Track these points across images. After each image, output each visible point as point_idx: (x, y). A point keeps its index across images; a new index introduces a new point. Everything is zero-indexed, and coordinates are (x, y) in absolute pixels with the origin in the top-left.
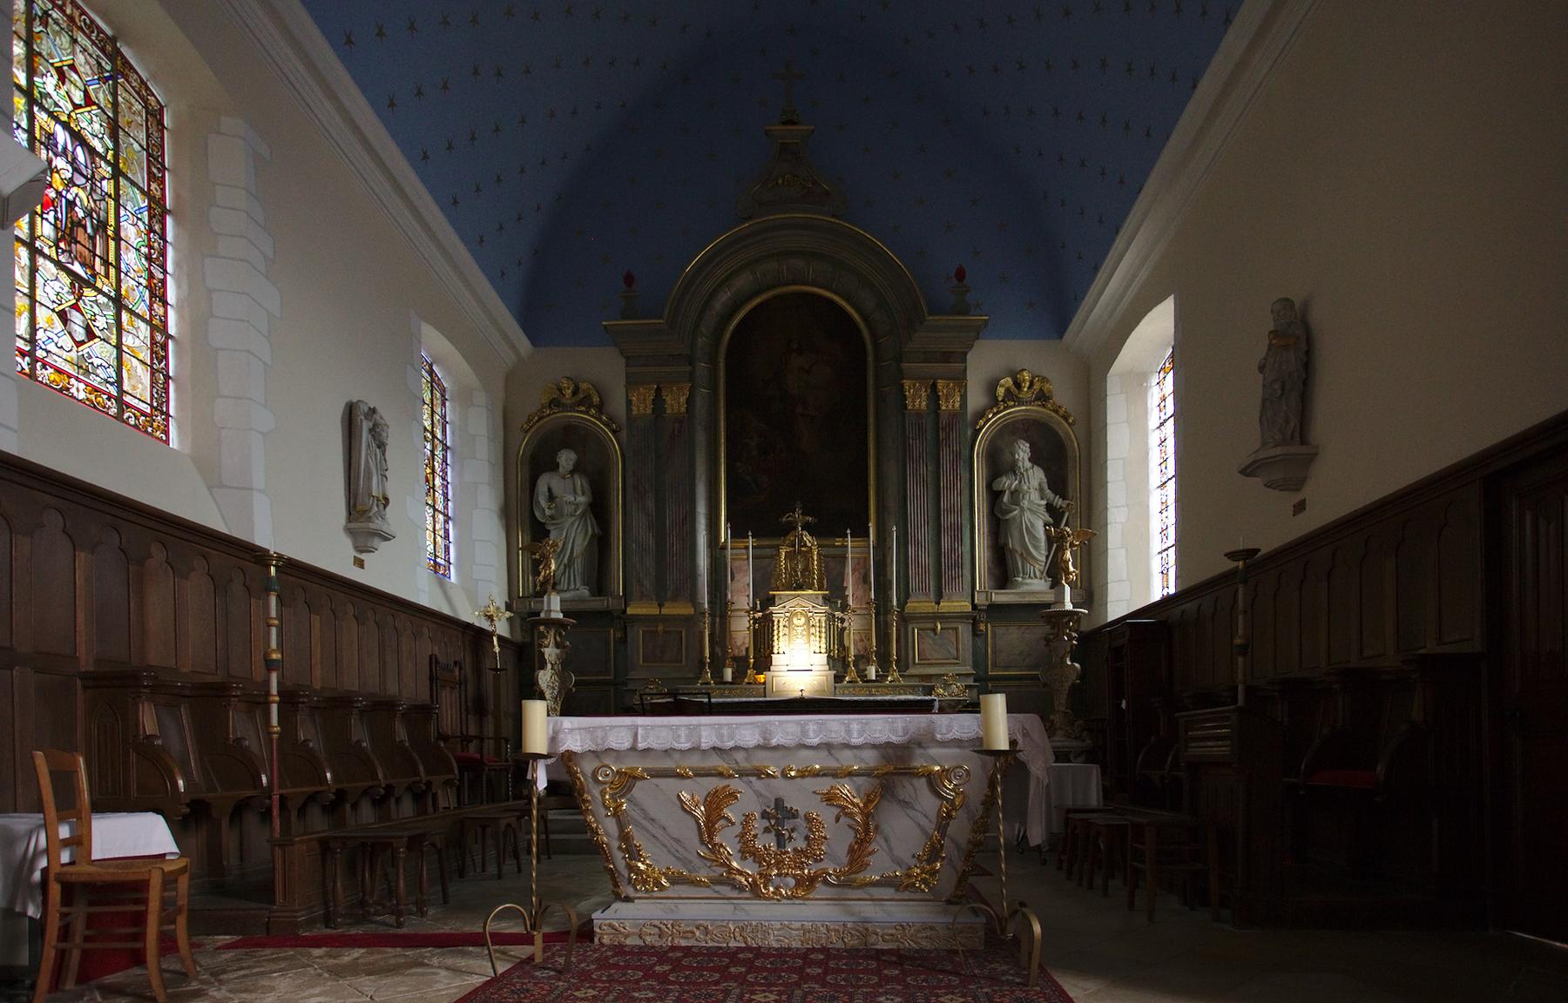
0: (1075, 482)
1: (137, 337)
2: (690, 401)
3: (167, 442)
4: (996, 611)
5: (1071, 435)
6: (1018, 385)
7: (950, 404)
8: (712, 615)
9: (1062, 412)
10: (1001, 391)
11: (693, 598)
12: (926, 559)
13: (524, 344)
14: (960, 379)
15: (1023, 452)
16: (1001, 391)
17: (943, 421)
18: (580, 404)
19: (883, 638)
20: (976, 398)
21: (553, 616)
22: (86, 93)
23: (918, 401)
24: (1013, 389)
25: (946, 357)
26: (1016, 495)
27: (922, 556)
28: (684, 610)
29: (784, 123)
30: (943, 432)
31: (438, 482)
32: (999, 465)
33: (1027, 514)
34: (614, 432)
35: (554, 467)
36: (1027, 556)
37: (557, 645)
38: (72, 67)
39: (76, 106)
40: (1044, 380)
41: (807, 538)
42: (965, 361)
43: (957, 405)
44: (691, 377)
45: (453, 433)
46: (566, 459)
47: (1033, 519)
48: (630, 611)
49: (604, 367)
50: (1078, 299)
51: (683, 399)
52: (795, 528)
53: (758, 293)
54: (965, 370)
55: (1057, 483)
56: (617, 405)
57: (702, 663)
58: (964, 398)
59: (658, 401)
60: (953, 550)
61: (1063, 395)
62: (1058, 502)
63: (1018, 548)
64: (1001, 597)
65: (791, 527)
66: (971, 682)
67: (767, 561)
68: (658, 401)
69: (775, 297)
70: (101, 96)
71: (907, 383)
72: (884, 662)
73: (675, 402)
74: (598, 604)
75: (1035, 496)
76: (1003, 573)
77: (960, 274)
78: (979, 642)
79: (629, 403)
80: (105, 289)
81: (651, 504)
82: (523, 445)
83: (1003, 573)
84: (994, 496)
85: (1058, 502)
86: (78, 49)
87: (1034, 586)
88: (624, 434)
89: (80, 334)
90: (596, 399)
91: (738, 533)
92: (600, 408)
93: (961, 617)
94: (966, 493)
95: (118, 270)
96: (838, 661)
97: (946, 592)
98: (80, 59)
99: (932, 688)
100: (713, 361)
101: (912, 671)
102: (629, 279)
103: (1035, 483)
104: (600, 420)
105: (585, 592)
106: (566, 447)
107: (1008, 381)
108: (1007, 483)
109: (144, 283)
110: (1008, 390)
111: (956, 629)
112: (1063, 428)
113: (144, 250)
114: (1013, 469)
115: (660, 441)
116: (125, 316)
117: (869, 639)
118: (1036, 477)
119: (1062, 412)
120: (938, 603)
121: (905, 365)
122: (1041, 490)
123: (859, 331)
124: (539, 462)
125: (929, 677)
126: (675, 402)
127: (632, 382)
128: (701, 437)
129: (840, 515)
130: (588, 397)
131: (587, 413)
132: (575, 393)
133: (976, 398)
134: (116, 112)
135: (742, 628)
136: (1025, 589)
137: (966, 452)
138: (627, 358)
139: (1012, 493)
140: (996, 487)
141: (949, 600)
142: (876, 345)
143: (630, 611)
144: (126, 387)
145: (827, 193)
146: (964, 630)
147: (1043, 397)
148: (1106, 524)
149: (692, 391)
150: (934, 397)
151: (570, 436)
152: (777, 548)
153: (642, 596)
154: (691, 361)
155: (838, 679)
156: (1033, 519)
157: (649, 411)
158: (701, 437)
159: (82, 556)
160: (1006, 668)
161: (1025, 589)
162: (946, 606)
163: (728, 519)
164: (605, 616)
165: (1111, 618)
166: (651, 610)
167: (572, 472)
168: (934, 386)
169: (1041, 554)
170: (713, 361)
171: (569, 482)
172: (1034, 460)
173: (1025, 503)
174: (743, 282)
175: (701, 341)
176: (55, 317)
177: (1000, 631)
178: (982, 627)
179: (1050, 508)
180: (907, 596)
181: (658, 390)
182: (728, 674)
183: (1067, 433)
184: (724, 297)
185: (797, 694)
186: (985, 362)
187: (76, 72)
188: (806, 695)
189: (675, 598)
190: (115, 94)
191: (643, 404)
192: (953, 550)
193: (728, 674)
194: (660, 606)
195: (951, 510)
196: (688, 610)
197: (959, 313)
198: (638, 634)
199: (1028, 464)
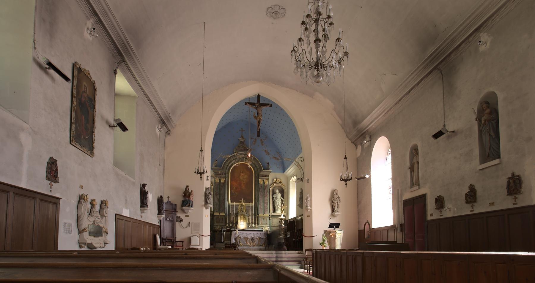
4: (273, 216)
5: (285, 191)
7: (266, 183)
12: (262, 207)
14: (268, 179)
15: (277, 191)
20: (270, 181)
25: (266, 176)
26: (276, 198)
27: (261, 207)
32: (274, 193)
36: (278, 208)
47: (279, 201)
55: (283, 196)
59: (220, 180)
64: (274, 214)
68: (220, 180)
72: (255, 224)
76: (274, 211)
77: (268, 164)
83: (274, 211)
84: (273, 198)
96: (248, 224)
108: (275, 196)
112: (283, 187)
118: (280, 195)
126: (223, 181)
128: (226, 186)
133: (270, 181)
135: (232, 218)
146: (268, 219)
147: (280, 182)
148: (392, 162)
150: (264, 182)
156: (279, 201)
159: (292, 214)
165: (290, 218)
166: (218, 214)
182: (231, 225)
186: (271, 176)
193: (231, 225)
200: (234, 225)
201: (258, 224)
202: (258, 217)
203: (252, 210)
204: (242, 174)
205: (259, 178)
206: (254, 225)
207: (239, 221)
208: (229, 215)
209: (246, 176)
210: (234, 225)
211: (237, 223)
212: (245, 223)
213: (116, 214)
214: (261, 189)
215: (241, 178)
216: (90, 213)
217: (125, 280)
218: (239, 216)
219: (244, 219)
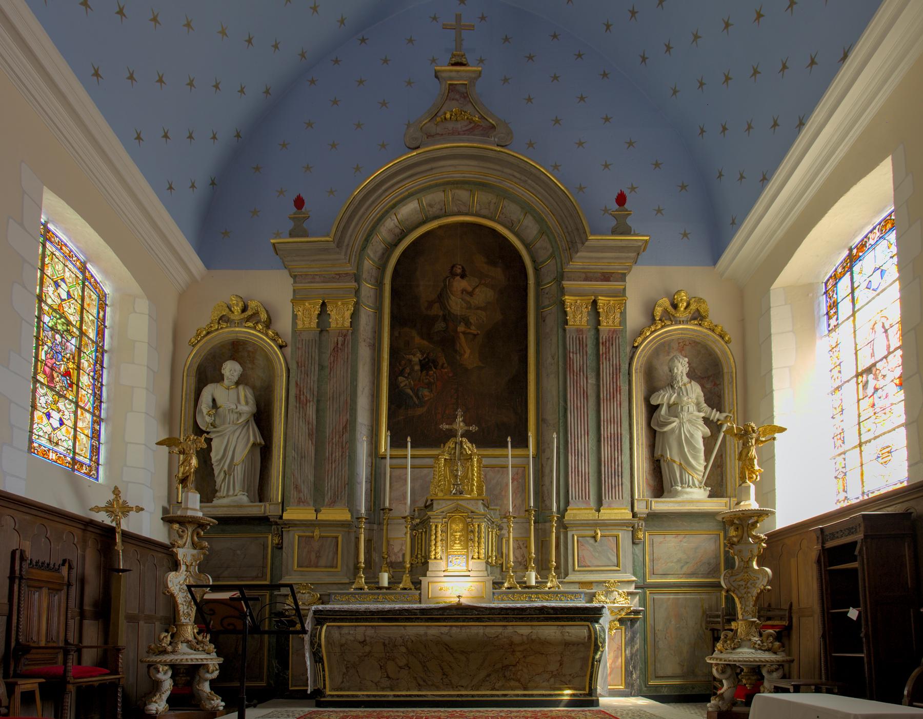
0: (731, 396)
1: (86, 420)
2: (355, 316)
3: (97, 479)
4: (654, 518)
5: (729, 354)
6: (675, 306)
8: (369, 521)
9: (718, 330)
10: (658, 311)
11: (351, 505)
12: (588, 467)
13: (196, 264)
15: (681, 367)
16: (658, 311)
17: (603, 336)
18: (248, 319)
19: (543, 545)
20: (634, 316)
21: (190, 513)
22: (68, 293)
23: (578, 318)
24: (670, 309)
25: (606, 277)
26: (674, 410)
27: (583, 465)
28: (342, 515)
29: (453, 65)
30: (600, 344)
31: (85, 380)
33: (687, 426)
34: (281, 347)
35: (220, 378)
36: (686, 465)
37: (194, 545)
38: (63, 280)
39: (63, 300)
40: (700, 300)
41: (468, 447)
42: (625, 281)
43: (617, 321)
44: (357, 292)
45: (111, 337)
46: (231, 369)
48: (286, 516)
49: (273, 289)
50: (736, 224)
51: (348, 314)
52: (455, 436)
53: (424, 222)
54: (624, 289)
55: (714, 400)
56: (284, 324)
57: (357, 568)
58: (623, 314)
60: (612, 459)
61: (719, 312)
62: (715, 415)
63: (677, 459)
64: (662, 505)
65: (451, 434)
66: (632, 589)
67: (425, 471)
69: (440, 227)
70: (76, 293)
71: (568, 299)
72: (543, 568)
73: (340, 317)
74: (257, 510)
75: (693, 408)
76: (660, 484)
78: (638, 549)
79: (295, 317)
80: (71, 398)
81: (311, 411)
82: (190, 357)
83: (660, 484)
84: (652, 409)
85: (715, 415)
86: (67, 270)
87: (694, 496)
88: (288, 350)
89: (56, 424)
90: (263, 316)
91: (397, 442)
92: (268, 324)
93: (621, 524)
94: (625, 404)
95: (78, 386)
96: (497, 570)
97: (605, 501)
98: (68, 274)
99: (594, 595)
100: (379, 284)
101: (572, 577)
102: (299, 203)
103: (693, 396)
104: (267, 335)
105: (244, 499)
106: (233, 358)
107: (665, 302)
108: (663, 398)
109: (90, 392)
110: (665, 311)
111: (617, 537)
112: (719, 346)
113: (92, 374)
114: (671, 384)
115: (324, 348)
116: (79, 411)
117: (528, 547)
118: (695, 392)
119: (718, 330)
120: (599, 511)
121: (566, 283)
122: (698, 404)
123: (520, 258)
124: (207, 373)
125: (590, 584)
127: (296, 300)
129: (503, 424)
130: (256, 314)
131: (254, 328)
132: (244, 310)
134: (83, 300)
135: (400, 539)
136: (685, 497)
137: (625, 367)
138: (294, 277)
139: (669, 406)
140: (654, 402)
141: (610, 507)
142: (537, 270)
143: (286, 516)
144: (77, 451)
145: (493, 127)
146: (625, 537)
147: (698, 317)
149: (357, 305)
151: (236, 350)
152: (436, 457)
153: (301, 502)
154: (357, 278)
155: (497, 584)
157: (314, 325)
158: (364, 352)
160: (665, 575)
161: (685, 497)
162: (606, 514)
163: (389, 428)
164: (263, 521)
165: (777, 528)
166: (307, 514)
167: (237, 384)
168: (595, 303)
169: (699, 464)
170: (379, 284)
171: (233, 393)
172: (691, 375)
173: (685, 416)
174: (409, 209)
175: (368, 264)
176: (44, 416)
177: (658, 539)
178: (640, 535)
179: (707, 421)
180: (567, 503)
181: (324, 305)
182: (385, 579)
183: (724, 353)
184: (390, 223)
185: (455, 601)
186: (642, 284)
187: (65, 282)
188: (464, 601)
189: (333, 503)
190: (83, 291)
191: (308, 321)
192: (612, 459)
193: (385, 579)
194: (317, 511)
195: (611, 421)
196: (345, 516)
197: (622, 234)
198: (292, 538)
199: (686, 379)
200: (406, 581)
201: (562, 571)
202: (563, 526)
203: (521, 489)
204: (460, 284)
205: (562, 291)
206: (532, 577)
207: (438, 550)
208: (378, 512)
209: (484, 295)
210: (406, 581)
211: (421, 566)
212: (476, 566)
213: (189, 587)
214: (576, 359)
215: (456, 305)
216: (82, 581)
217: (442, 709)
218: (438, 526)
219: (469, 537)
